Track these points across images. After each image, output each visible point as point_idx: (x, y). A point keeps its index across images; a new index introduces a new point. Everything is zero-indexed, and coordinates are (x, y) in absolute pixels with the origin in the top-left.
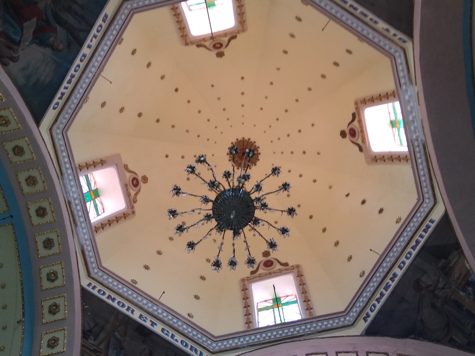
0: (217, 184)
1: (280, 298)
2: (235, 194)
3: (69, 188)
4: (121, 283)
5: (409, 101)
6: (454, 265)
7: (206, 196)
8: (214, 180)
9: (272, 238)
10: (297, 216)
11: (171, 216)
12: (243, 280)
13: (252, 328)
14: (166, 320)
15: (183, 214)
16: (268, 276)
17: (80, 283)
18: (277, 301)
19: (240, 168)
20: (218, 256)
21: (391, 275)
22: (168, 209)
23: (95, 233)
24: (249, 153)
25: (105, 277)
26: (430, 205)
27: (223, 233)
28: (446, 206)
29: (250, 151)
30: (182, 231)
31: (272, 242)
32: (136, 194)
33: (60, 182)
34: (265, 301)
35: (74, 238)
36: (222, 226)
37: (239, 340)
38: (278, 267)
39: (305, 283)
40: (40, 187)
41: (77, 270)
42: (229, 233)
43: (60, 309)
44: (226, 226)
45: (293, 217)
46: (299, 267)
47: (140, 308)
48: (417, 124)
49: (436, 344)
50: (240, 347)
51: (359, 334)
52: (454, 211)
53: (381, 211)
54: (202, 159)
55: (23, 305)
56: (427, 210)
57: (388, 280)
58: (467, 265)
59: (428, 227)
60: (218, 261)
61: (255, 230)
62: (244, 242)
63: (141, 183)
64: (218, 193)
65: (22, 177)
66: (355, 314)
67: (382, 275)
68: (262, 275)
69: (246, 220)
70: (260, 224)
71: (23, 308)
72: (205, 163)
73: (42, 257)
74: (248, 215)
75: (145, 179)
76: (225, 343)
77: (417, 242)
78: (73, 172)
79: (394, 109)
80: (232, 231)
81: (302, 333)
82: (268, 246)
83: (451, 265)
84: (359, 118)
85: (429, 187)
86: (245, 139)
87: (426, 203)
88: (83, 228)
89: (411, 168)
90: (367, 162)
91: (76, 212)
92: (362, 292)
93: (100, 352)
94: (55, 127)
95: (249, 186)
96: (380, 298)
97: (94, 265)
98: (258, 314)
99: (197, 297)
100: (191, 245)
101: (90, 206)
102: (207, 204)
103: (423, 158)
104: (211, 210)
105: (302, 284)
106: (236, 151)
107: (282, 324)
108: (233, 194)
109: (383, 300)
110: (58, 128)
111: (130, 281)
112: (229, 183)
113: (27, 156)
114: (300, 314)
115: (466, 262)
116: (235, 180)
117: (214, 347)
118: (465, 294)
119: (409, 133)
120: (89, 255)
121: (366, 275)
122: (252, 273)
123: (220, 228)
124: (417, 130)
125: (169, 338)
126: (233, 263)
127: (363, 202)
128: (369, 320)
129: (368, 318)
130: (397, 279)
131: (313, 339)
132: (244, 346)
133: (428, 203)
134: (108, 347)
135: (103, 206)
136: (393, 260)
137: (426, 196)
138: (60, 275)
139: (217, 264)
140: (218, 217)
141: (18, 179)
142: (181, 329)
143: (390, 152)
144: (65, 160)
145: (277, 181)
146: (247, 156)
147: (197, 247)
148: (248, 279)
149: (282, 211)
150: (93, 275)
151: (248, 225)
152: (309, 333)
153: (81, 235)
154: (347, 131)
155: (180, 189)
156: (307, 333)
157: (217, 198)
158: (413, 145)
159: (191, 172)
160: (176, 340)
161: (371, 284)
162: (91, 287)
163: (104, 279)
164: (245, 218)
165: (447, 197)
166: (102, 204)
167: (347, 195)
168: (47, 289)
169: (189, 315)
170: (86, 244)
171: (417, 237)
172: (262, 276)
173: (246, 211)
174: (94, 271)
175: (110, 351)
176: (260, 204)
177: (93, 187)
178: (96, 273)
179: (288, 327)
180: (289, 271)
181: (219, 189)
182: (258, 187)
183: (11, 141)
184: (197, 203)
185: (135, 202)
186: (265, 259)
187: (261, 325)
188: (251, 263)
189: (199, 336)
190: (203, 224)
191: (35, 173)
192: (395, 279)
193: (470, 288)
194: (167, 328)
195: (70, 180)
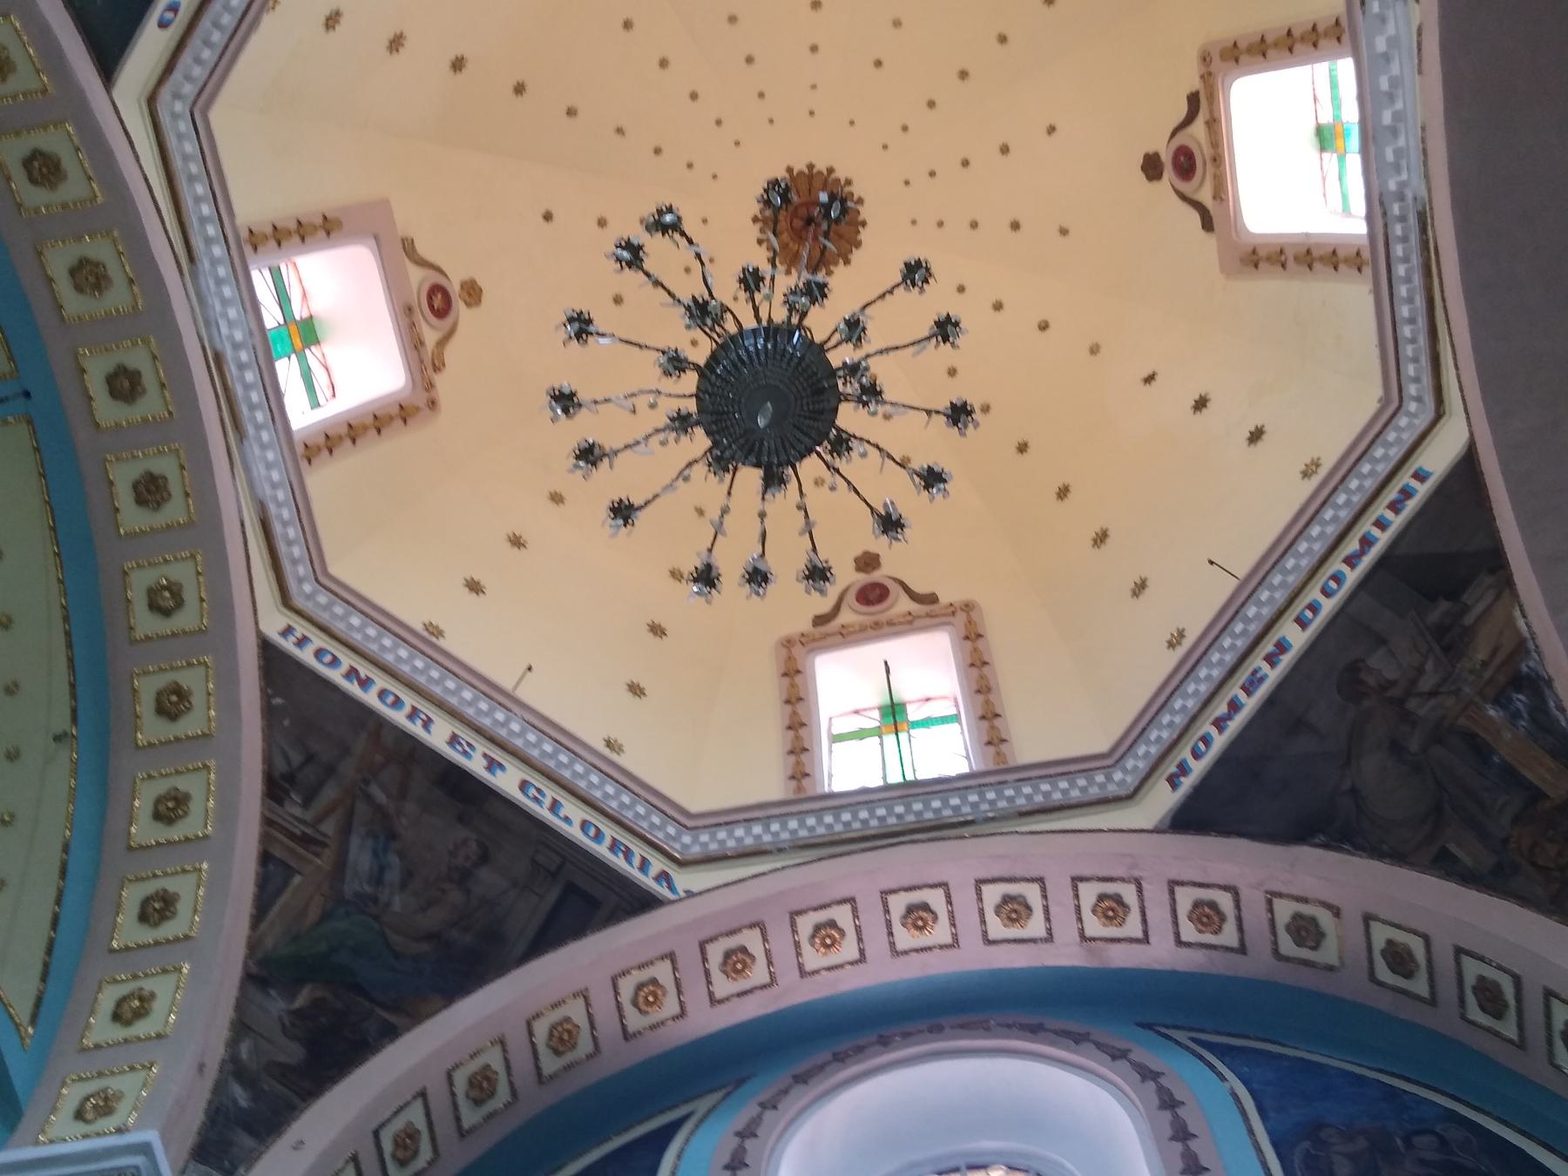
0: (715, 307)
1: (903, 705)
2: (775, 346)
3: (218, 307)
4: (389, 630)
5: (1386, 57)
6: (1479, 618)
7: (676, 351)
8: (706, 296)
9: (892, 503)
10: (978, 429)
11: (559, 411)
12: (788, 643)
13: (810, 793)
14: (533, 756)
15: (599, 407)
16: (870, 632)
17: (257, 623)
18: (894, 714)
19: (793, 271)
20: (710, 550)
21: (1268, 646)
22: (547, 385)
23: (304, 464)
24: (827, 208)
25: (339, 609)
26: (1421, 423)
27: (728, 477)
28: (1475, 428)
29: (832, 197)
30: (594, 464)
31: (889, 515)
32: (442, 343)
33: (184, 285)
34: (857, 712)
35: (237, 479)
36: (727, 454)
37: (767, 828)
38: (904, 604)
39: (987, 660)
40: (117, 297)
41: (242, 546)
42: (750, 477)
43: (193, 703)
44: (739, 453)
45: (962, 434)
46: (972, 610)
47: (452, 716)
48: (1407, 140)
49: (1392, 865)
50: (768, 848)
51: (1149, 826)
52: (1497, 444)
53: (1256, 436)
54: (668, 218)
55: (73, 686)
56: (1408, 438)
57: (1257, 662)
58: (1521, 623)
59: (1407, 493)
60: (709, 567)
61: (837, 471)
62: (799, 508)
63: (459, 305)
64: (716, 342)
65: (59, 262)
66: (1141, 765)
67: (1241, 644)
68: (851, 629)
69: (806, 434)
70: (854, 454)
71: (74, 696)
72: (677, 236)
73: (132, 535)
74: (814, 419)
75: (473, 292)
76: (722, 835)
77: (1367, 542)
78: (229, 254)
79: (1334, 85)
80: (759, 473)
81: (968, 814)
82: (876, 525)
83: (1469, 620)
84: (1211, 111)
85: (1425, 361)
86: (815, 171)
87: (1409, 414)
88: (263, 447)
89: (1370, 291)
90: (1224, 269)
91: (239, 391)
92: (1172, 693)
93: (324, 845)
94: (165, 94)
95: (822, 322)
96: (1228, 717)
97: (301, 570)
98: (830, 751)
99: (636, 690)
100: (623, 512)
101: (287, 371)
102: (679, 377)
103: (1415, 260)
104: (691, 396)
105: (978, 663)
106: (785, 196)
107: (906, 785)
108: (769, 346)
109: (1235, 725)
110: (177, 96)
111: (419, 628)
112: (756, 309)
113: (73, 188)
114: (968, 757)
115: (1517, 613)
116: (778, 298)
117: (685, 846)
118: (1501, 713)
119: (1377, 170)
120: (286, 535)
121: (1187, 643)
122: (820, 620)
123: (721, 461)
124: (1404, 163)
125: (543, 812)
126: (757, 577)
127: (1201, 404)
128: (1187, 783)
129: (1182, 779)
130: (1286, 660)
131: (1002, 834)
132: (781, 846)
133: (1415, 415)
134: (346, 830)
135: (329, 376)
136: (1280, 597)
137: (1412, 389)
138: (189, 595)
139: (706, 577)
140: (715, 423)
141: (43, 267)
142: (582, 784)
143: (1307, 235)
144: (196, 191)
145: (919, 311)
146: (821, 216)
147: (641, 518)
148: (803, 640)
149: (929, 412)
150: (299, 602)
151: (814, 455)
152: (990, 815)
153: (259, 470)
154: (1166, 158)
155: (589, 322)
156: (984, 815)
157: (714, 358)
158: (1385, 214)
159: (630, 264)
160: (567, 819)
161: (1203, 672)
162: (292, 639)
163: (335, 616)
164: (805, 429)
165: (1478, 391)
166: (327, 370)
167: (1150, 379)
168: (148, 638)
169: (609, 744)
170: (275, 499)
171: (1366, 526)
172: (847, 634)
173: (808, 404)
174: (303, 589)
175: (355, 841)
176: (857, 385)
177: (298, 311)
178: (309, 597)
179: (923, 794)
180: (937, 620)
181: (723, 328)
182: (854, 329)
183: (17, 134)
184: (647, 369)
185: (439, 369)
186: (862, 579)
187: (839, 785)
188: (818, 579)
189: (641, 810)
190: (663, 443)
191: (99, 250)
192: (1281, 657)
193: (1520, 697)
194: (537, 781)
195: (219, 282)
